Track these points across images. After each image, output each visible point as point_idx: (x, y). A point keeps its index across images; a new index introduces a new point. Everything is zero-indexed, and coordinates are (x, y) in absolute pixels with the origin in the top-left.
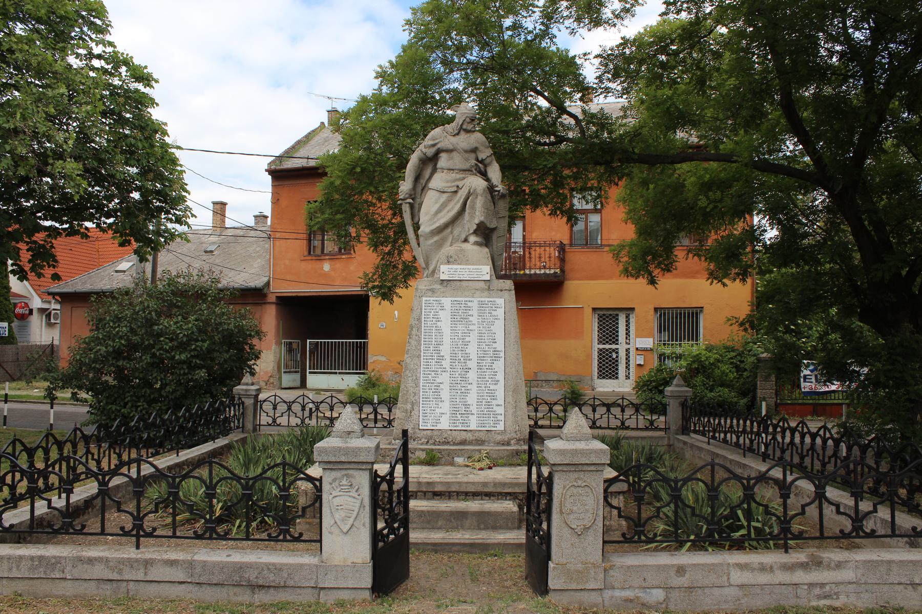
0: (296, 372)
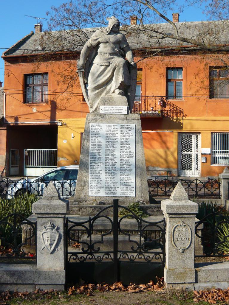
0: (16, 167)
